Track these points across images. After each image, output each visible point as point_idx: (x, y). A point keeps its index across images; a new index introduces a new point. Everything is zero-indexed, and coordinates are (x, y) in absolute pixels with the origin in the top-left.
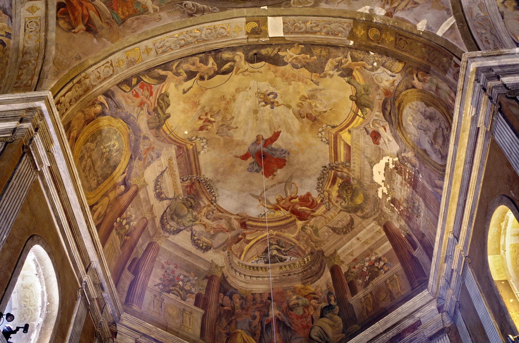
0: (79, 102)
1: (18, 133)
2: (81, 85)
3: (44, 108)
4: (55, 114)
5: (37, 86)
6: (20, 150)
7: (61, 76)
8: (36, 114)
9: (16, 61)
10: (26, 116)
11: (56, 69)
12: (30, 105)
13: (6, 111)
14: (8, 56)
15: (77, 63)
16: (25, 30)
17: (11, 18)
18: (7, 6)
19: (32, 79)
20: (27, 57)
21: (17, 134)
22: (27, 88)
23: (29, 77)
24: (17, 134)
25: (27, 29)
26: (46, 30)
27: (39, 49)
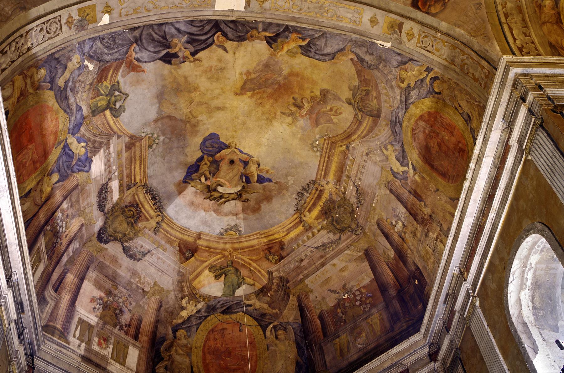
0: (530, 24)
1: (536, 109)
2: (511, 14)
3: (519, 70)
4: (531, 61)
5: (491, 65)
6: (555, 117)
7: (491, 34)
8: (523, 81)
9: (458, 74)
10: (520, 92)
11: (482, 36)
12: (509, 83)
13: (506, 109)
14: (450, 79)
15: (484, 9)
16: (428, 51)
17: (411, 60)
18: (399, 58)
19: (483, 67)
20: (458, 61)
21: (536, 110)
22: (490, 77)
23: (479, 69)
24: (536, 110)
25: (428, 49)
26: (436, 29)
27: (453, 46)
